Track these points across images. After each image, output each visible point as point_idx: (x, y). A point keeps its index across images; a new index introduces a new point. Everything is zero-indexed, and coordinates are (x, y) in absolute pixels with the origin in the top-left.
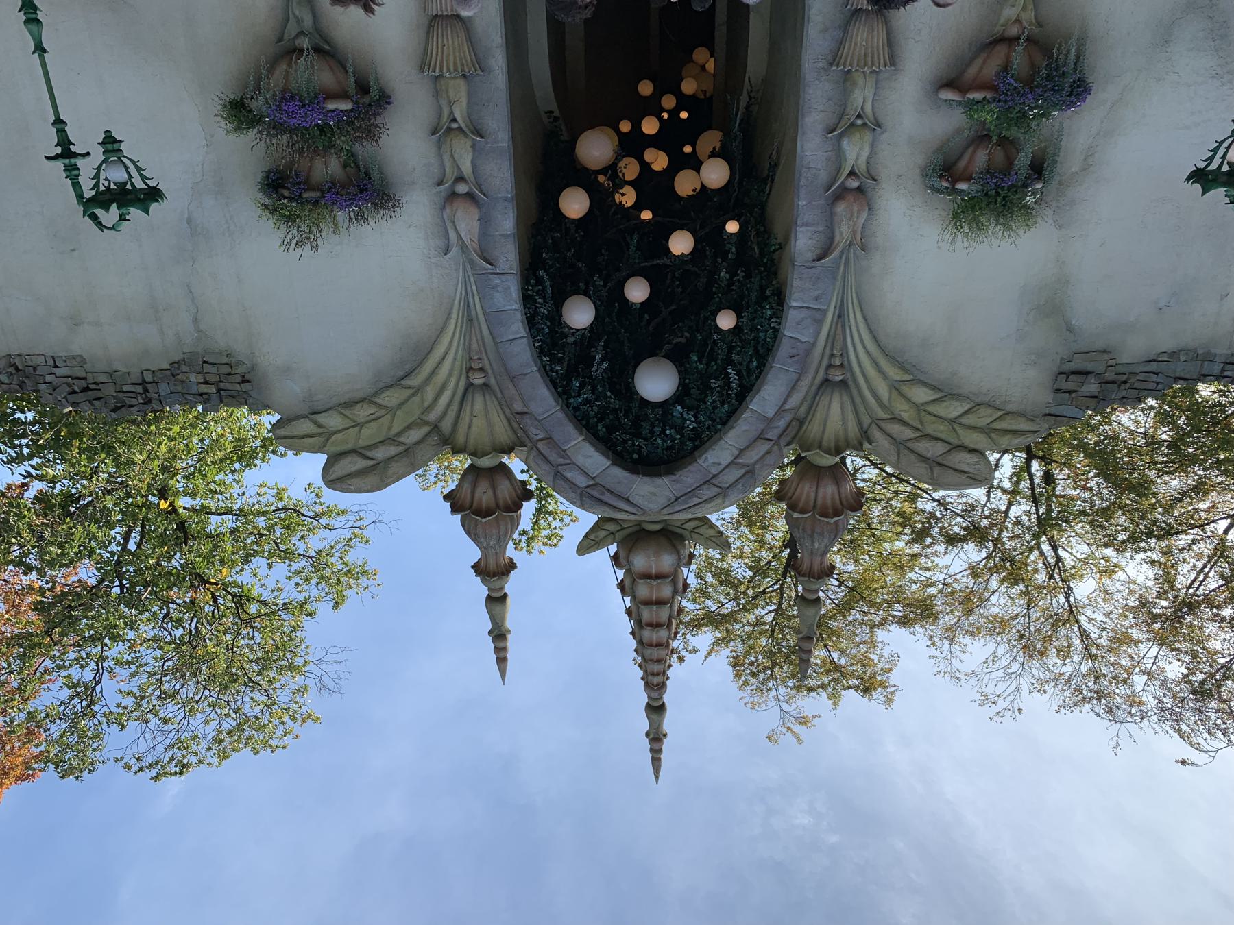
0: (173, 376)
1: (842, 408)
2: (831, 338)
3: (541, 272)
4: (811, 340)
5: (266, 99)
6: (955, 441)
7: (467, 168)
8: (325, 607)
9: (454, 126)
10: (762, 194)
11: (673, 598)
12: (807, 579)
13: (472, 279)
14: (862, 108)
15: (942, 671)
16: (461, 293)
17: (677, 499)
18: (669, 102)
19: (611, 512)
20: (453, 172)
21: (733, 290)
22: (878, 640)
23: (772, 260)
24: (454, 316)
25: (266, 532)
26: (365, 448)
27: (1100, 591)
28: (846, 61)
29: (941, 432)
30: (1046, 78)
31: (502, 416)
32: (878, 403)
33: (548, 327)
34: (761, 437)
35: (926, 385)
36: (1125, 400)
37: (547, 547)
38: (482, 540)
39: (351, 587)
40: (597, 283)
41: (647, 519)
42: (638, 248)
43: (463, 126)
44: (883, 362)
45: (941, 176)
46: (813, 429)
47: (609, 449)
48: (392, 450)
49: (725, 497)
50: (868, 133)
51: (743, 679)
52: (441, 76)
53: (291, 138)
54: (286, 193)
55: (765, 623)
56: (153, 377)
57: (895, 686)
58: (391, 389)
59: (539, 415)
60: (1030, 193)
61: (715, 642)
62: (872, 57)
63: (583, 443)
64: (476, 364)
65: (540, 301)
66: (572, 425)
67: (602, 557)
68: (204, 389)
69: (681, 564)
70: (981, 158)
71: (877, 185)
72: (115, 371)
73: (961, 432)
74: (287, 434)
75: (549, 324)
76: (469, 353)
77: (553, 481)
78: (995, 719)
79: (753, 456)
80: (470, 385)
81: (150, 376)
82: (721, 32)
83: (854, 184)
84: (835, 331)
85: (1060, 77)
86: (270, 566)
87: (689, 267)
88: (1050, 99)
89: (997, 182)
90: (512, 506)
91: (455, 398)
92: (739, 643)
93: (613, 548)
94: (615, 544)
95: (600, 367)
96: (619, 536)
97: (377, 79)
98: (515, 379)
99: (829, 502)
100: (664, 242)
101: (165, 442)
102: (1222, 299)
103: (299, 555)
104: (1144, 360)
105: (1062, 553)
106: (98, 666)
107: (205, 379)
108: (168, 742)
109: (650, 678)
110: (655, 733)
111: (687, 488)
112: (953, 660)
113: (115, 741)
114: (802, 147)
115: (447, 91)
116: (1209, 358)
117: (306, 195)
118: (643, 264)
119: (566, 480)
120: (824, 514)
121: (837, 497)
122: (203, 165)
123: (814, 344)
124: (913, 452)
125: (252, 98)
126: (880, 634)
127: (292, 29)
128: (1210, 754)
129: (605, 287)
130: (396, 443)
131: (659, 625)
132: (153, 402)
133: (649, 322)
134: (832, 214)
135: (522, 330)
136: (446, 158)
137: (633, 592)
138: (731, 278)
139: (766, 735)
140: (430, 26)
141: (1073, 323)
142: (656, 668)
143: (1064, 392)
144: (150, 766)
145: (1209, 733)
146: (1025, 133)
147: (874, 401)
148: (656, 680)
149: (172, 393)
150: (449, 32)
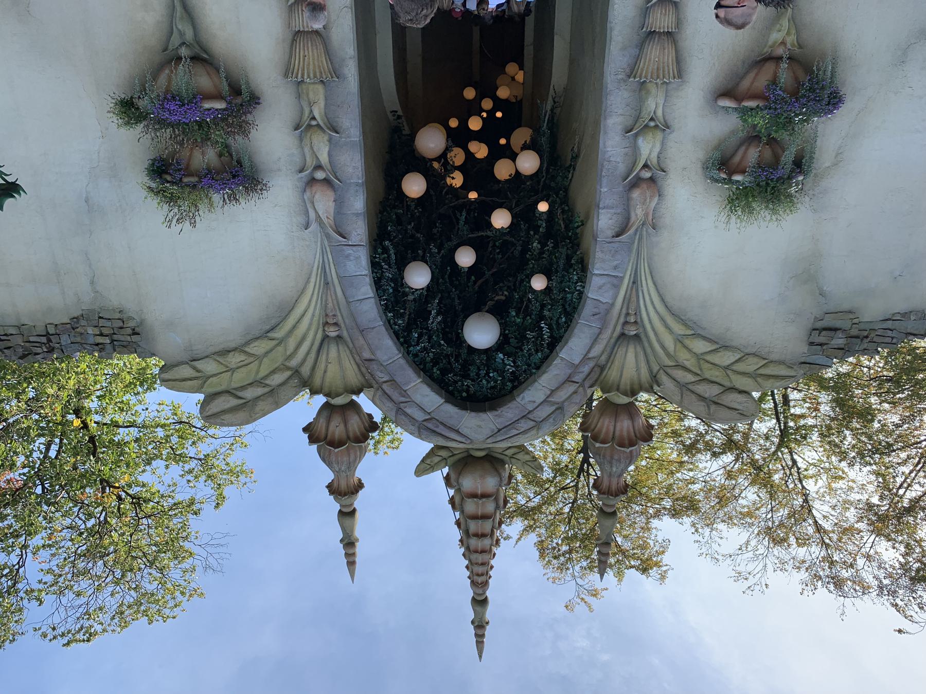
0: (73, 329)
1: (636, 357)
2: (627, 301)
4: (610, 302)
5: (151, 99)
6: (728, 384)
7: (324, 158)
8: (208, 509)
9: (314, 123)
10: (565, 179)
11: (495, 513)
12: (606, 496)
14: (655, 113)
15: (704, 554)
16: (319, 261)
17: (499, 430)
18: (487, 104)
19: (444, 441)
21: (544, 258)
22: (653, 527)
23: (576, 234)
24: (313, 280)
25: (164, 441)
26: (236, 389)
29: (717, 377)
30: (809, 90)
31: (352, 362)
32: (664, 352)
34: (569, 380)
35: (705, 338)
36: (866, 351)
37: (390, 449)
42: (466, 223)
43: (321, 123)
44: (670, 320)
45: (719, 169)
46: (612, 374)
47: (442, 388)
48: (259, 391)
49: (538, 429)
50: (659, 133)
51: (547, 559)
53: (174, 131)
54: (169, 178)
56: (56, 330)
57: (667, 565)
58: (259, 341)
60: (794, 184)
61: (525, 530)
62: (663, 71)
65: (386, 267)
66: (411, 370)
67: (437, 477)
68: (100, 340)
69: (503, 484)
70: (753, 154)
71: (666, 175)
72: (23, 325)
74: (170, 377)
75: (393, 285)
77: (396, 416)
78: (747, 592)
79: (562, 395)
80: (325, 337)
81: (53, 329)
83: (647, 174)
84: (630, 295)
85: (820, 89)
86: (167, 467)
87: (507, 238)
89: (767, 175)
90: (361, 437)
91: (313, 347)
92: (543, 531)
93: (446, 470)
94: (447, 467)
95: (435, 320)
96: (451, 461)
97: (247, 83)
99: (625, 434)
100: (487, 218)
101: (73, 377)
103: (191, 458)
104: (881, 319)
105: (795, 457)
106: (22, 552)
107: (101, 331)
108: (78, 615)
109: (476, 578)
110: (479, 622)
111: (507, 421)
113: (33, 613)
115: (308, 94)
117: (185, 180)
119: (406, 415)
122: (99, 153)
123: (613, 305)
124: (693, 392)
125: (139, 97)
126: (655, 523)
127: (175, 40)
128: (920, 624)
130: (263, 385)
131: (483, 536)
132: (55, 350)
133: (475, 282)
134: (629, 199)
135: (370, 291)
136: (307, 150)
137: (462, 508)
138: (542, 248)
139: (564, 605)
140: (294, 40)
141: (825, 288)
142: (480, 569)
144: (63, 635)
147: (662, 351)
148: (480, 580)
149: (72, 343)
150: (310, 45)
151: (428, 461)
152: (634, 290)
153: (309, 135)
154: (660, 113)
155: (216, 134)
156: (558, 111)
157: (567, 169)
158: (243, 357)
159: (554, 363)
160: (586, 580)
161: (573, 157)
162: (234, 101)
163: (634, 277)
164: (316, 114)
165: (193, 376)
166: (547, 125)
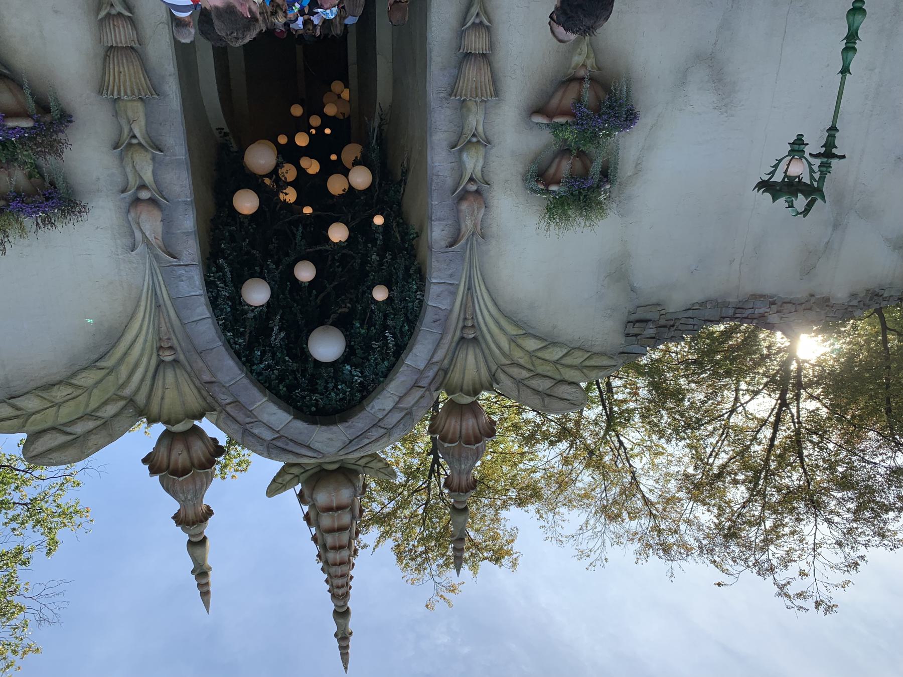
2: (464, 306)
3: (221, 261)
4: (449, 308)
6: (558, 377)
8: (38, 557)
9: (134, 141)
10: (398, 193)
12: (457, 493)
13: (158, 271)
15: (550, 537)
17: (351, 441)
19: (295, 458)
20: (136, 181)
21: (383, 269)
23: (412, 246)
24: (143, 303)
26: (64, 425)
27: (650, 464)
28: (461, 92)
29: (548, 371)
31: (192, 386)
32: (501, 352)
33: (230, 306)
34: (415, 385)
35: (535, 337)
38: (181, 495)
39: (65, 526)
40: (270, 267)
41: (326, 460)
42: (303, 238)
43: (143, 142)
44: (503, 322)
45: (537, 181)
46: (455, 377)
48: (91, 425)
51: (404, 562)
52: (119, 98)
55: (417, 515)
59: (225, 383)
61: (381, 536)
63: (267, 403)
64: (166, 344)
65: (222, 285)
67: (290, 495)
70: (565, 167)
73: (562, 370)
75: (230, 304)
76: (159, 334)
80: (160, 363)
82: (353, 70)
83: (472, 187)
88: (613, 123)
93: (299, 487)
94: (300, 484)
95: (277, 337)
97: (56, 100)
98: (203, 354)
99: (471, 432)
100: (324, 232)
102: (731, 264)
103: (14, 503)
105: (622, 438)
109: (336, 590)
112: (557, 527)
114: (432, 160)
115: (126, 112)
116: (725, 305)
118: (308, 250)
119: (254, 435)
120: (468, 443)
121: (477, 428)
123: (451, 311)
124: (528, 387)
126: (503, 513)
129: (277, 270)
130: (94, 418)
131: (341, 548)
133: (317, 296)
134: (458, 211)
135: (207, 312)
136: (129, 169)
138: (381, 259)
140: (106, 57)
141: (635, 285)
142: (340, 582)
143: (632, 336)
145: (735, 561)
146: (597, 148)
148: (340, 592)
150: (125, 61)
151: (280, 480)
152: (469, 296)
153: (130, 154)
154: (480, 129)
155: (23, 155)
156: (385, 127)
157: (399, 183)
158: (69, 390)
159: (401, 370)
160: (444, 578)
161: (403, 172)
162: (43, 120)
163: (469, 284)
164: (137, 132)
165: (12, 415)
166: (376, 141)
